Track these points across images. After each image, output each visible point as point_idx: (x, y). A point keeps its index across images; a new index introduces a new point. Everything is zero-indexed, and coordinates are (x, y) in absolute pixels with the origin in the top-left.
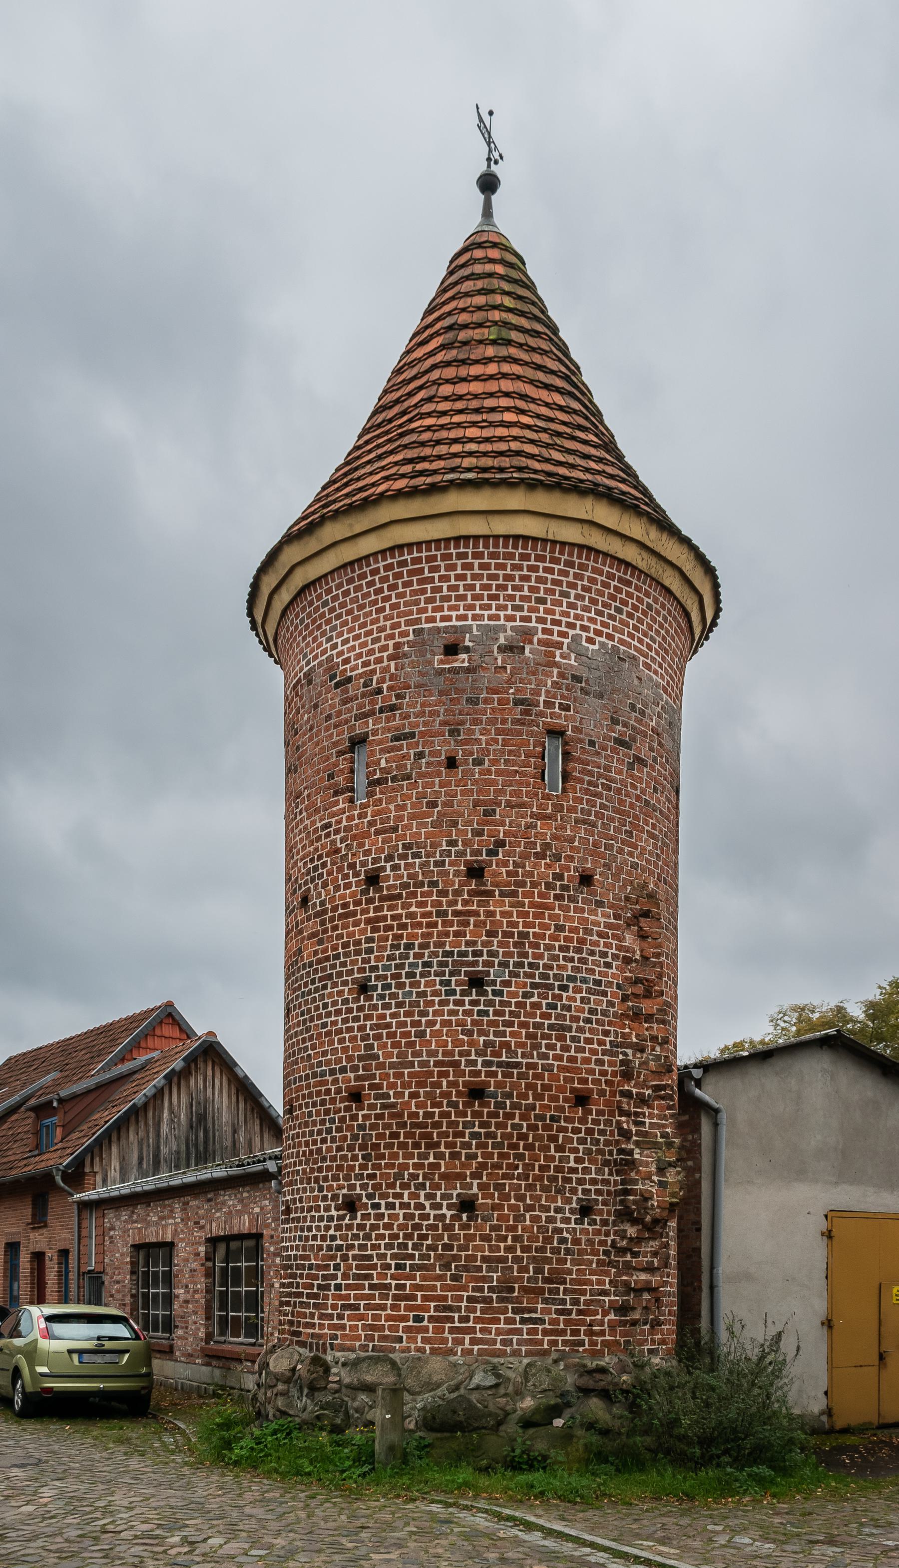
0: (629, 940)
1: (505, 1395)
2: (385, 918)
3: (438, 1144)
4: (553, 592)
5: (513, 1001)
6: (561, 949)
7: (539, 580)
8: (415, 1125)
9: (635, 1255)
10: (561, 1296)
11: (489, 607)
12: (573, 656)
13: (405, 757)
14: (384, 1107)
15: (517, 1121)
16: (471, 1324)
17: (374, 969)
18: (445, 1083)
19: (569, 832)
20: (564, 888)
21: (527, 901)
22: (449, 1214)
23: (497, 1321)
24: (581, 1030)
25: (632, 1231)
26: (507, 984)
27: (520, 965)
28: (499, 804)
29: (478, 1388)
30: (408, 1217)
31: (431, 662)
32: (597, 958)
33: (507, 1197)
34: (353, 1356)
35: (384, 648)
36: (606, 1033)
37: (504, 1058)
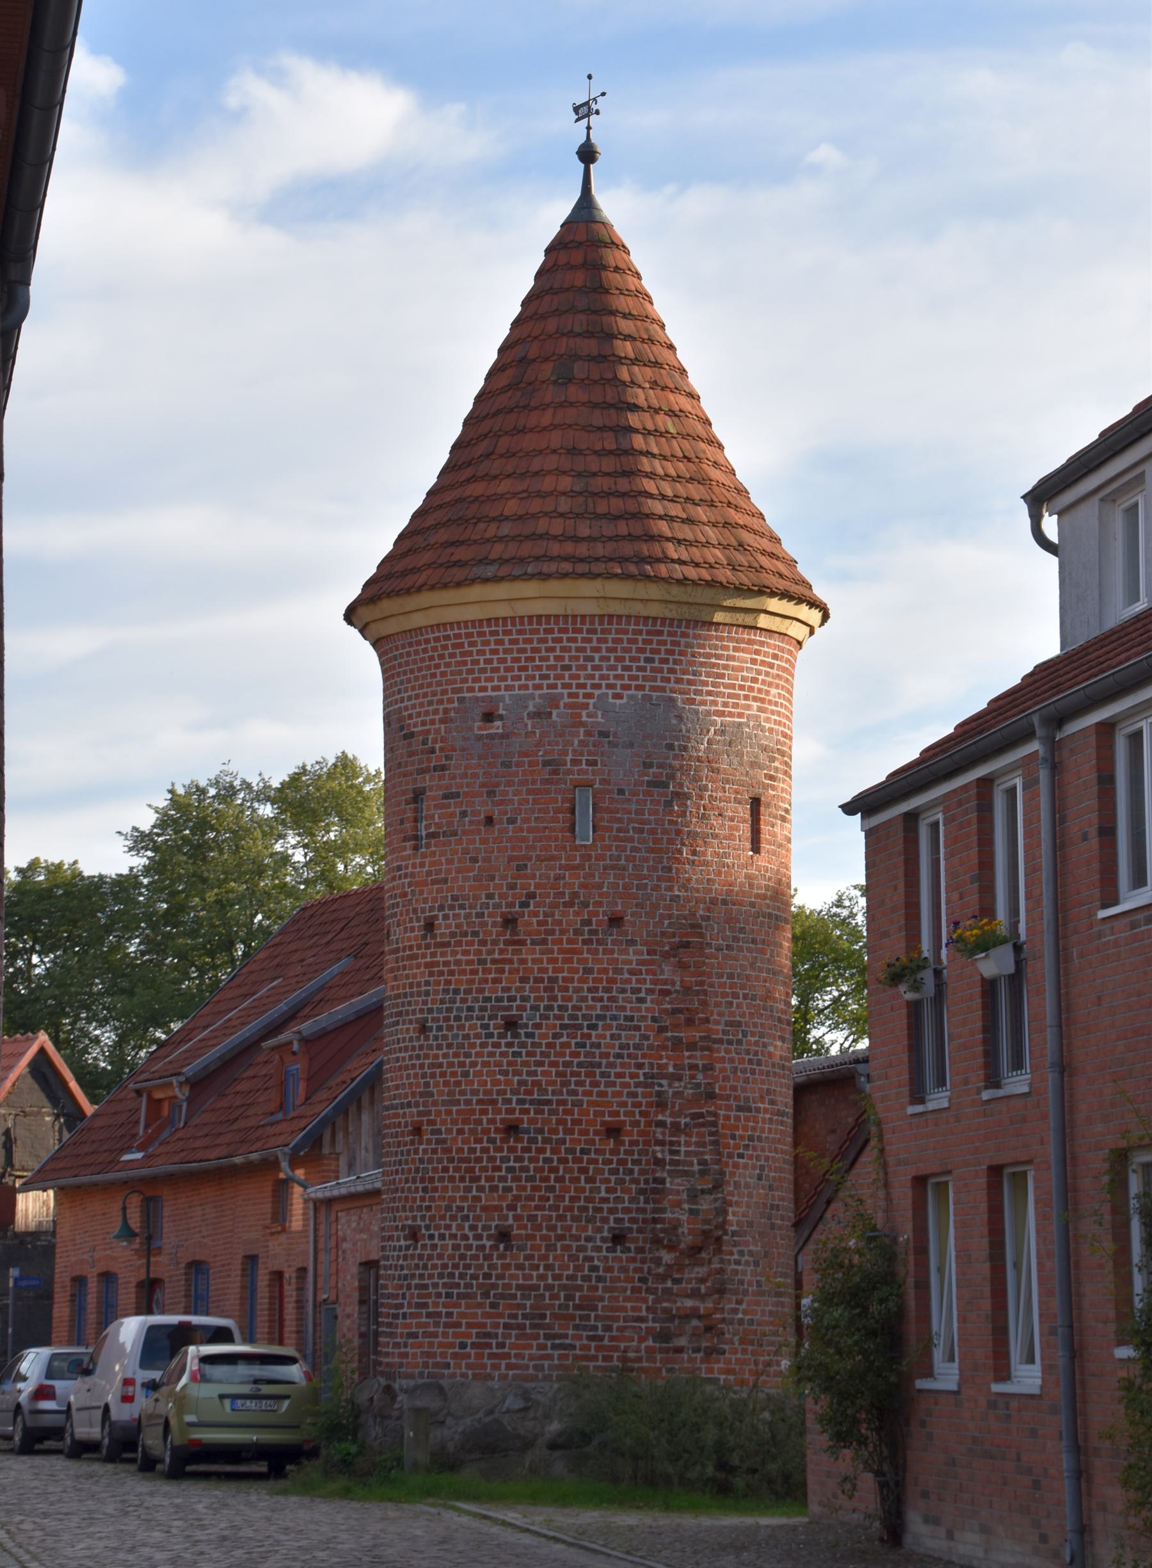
0: (667, 971)
1: (535, 1418)
2: (437, 964)
3: (478, 1179)
4: (577, 658)
5: (544, 1042)
6: (590, 990)
7: (563, 649)
8: (462, 1160)
9: (676, 1281)
10: (592, 1323)
11: (519, 678)
12: (599, 714)
13: (453, 815)
14: (438, 1142)
15: (548, 1155)
16: (506, 1350)
17: (430, 1011)
18: (485, 1121)
19: (597, 880)
20: (593, 932)
21: (556, 948)
22: (488, 1244)
23: (530, 1347)
24: (611, 1065)
25: (667, 1257)
26: (538, 1026)
27: (549, 1008)
28: (530, 859)
29: (508, 1411)
30: (456, 1247)
31: (471, 729)
32: (629, 995)
33: (539, 1228)
34: (412, 1383)
35: (436, 712)
36: (640, 1066)
37: (535, 1096)
